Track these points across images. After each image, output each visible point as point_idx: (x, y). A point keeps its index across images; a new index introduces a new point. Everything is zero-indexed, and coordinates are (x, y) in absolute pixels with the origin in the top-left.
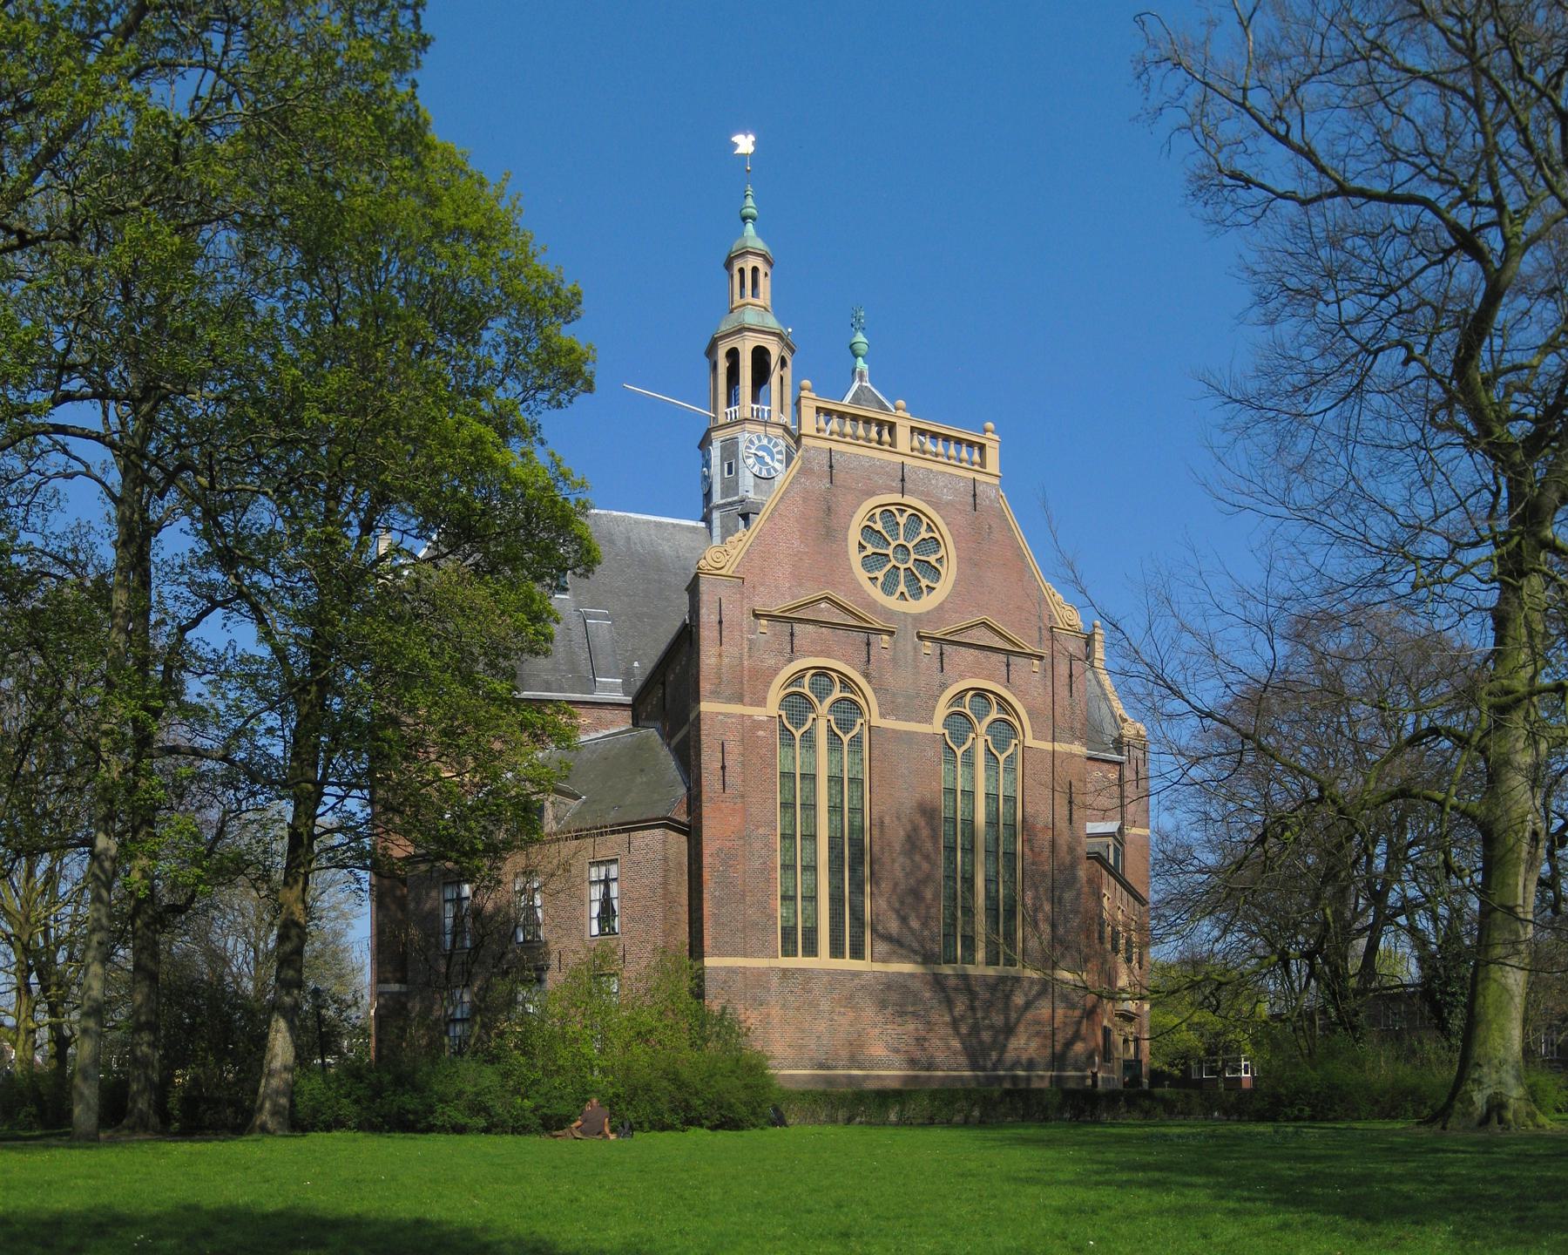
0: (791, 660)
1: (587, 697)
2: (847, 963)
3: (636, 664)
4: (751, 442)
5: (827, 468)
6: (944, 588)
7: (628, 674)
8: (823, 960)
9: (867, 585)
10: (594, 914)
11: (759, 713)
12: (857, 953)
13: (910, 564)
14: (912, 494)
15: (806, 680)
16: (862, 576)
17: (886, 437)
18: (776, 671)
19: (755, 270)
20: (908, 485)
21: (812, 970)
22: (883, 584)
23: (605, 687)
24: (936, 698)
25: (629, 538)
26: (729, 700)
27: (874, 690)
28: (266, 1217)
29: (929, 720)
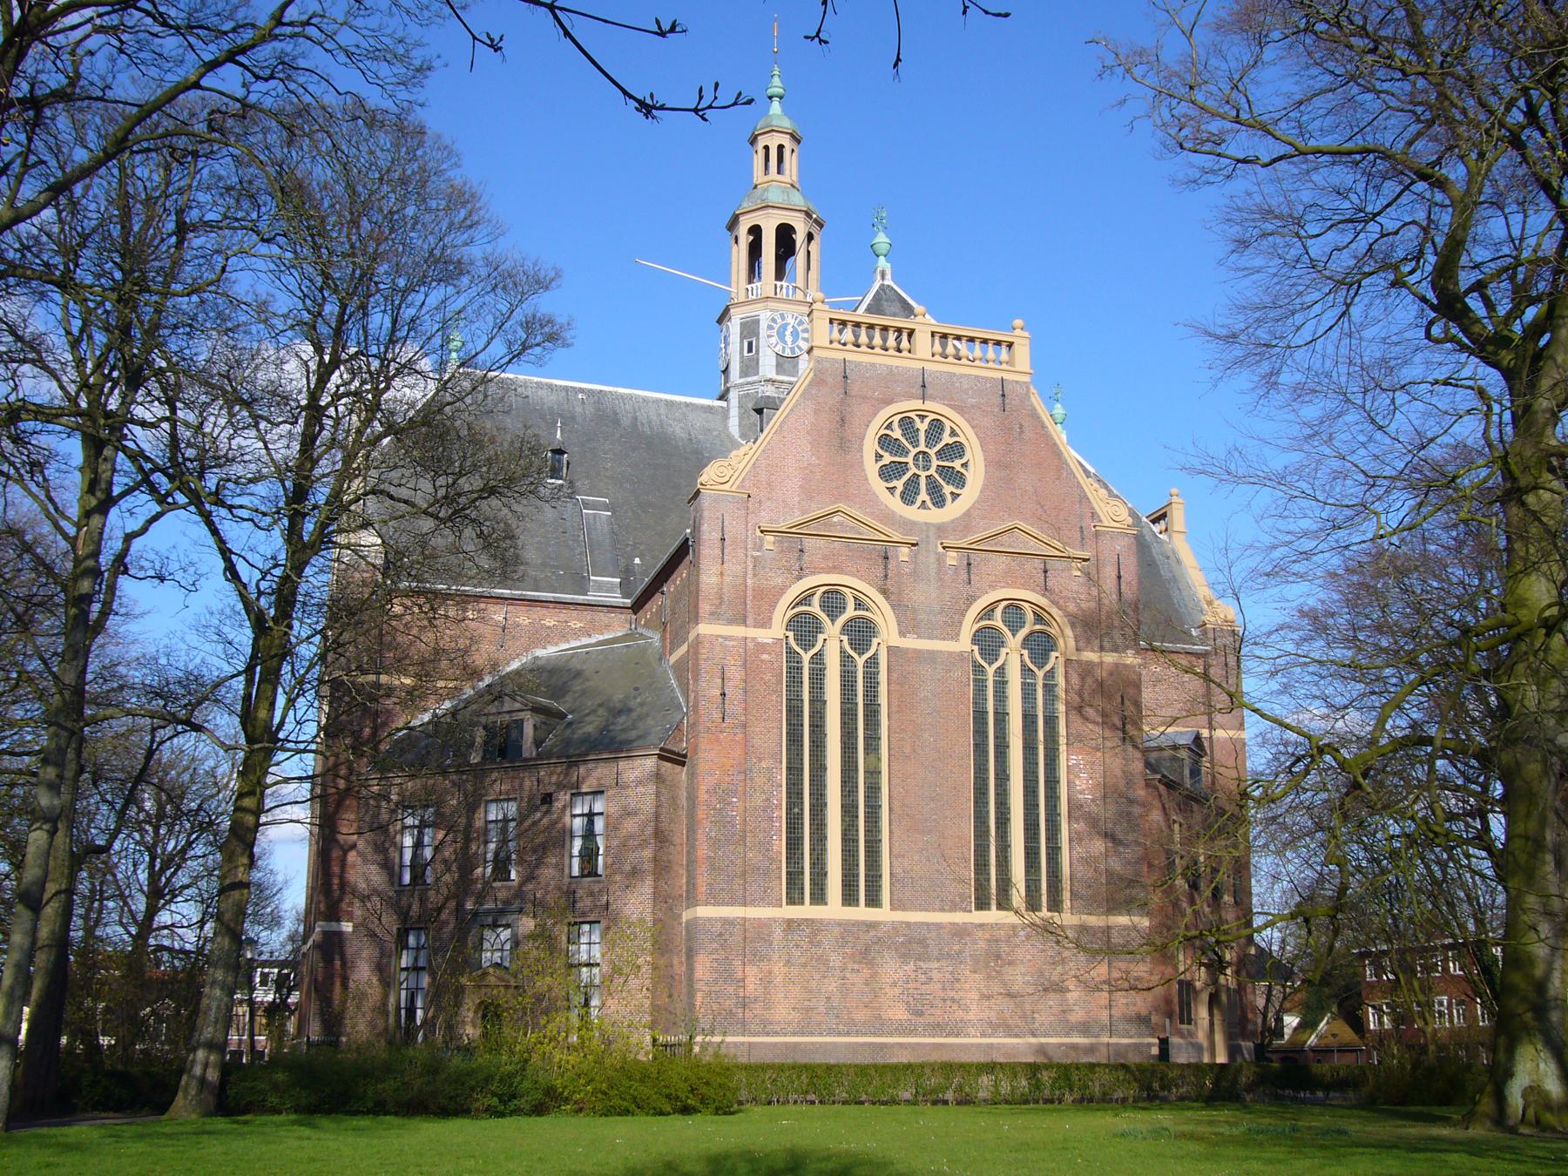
0: (800, 578)
1: (580, 598)
2: (861, 913)
3: (637, 561)
4: (774, 320)
5: (840, 378)
6: (970, 493)
7: (627, 574)
8: (834, 909)
9: (885, 496)
10: (576, 851)
11: (765, 636)
12: (873, 900)
13: (932, 471)
14: (933, 398)
15: (816, 600)
16: (879, 486)
17: (905, 344)
18: (783, 590)
19: (781, 147)
20: (929, 391)
21: (821, 921)
22: (903, 493)
23: (600, 587)
24: (963, 613)
25: (635, 418)
26: (730, 622)
27: (893, 607)
28: (1170, 598)
29: (955, 636)
